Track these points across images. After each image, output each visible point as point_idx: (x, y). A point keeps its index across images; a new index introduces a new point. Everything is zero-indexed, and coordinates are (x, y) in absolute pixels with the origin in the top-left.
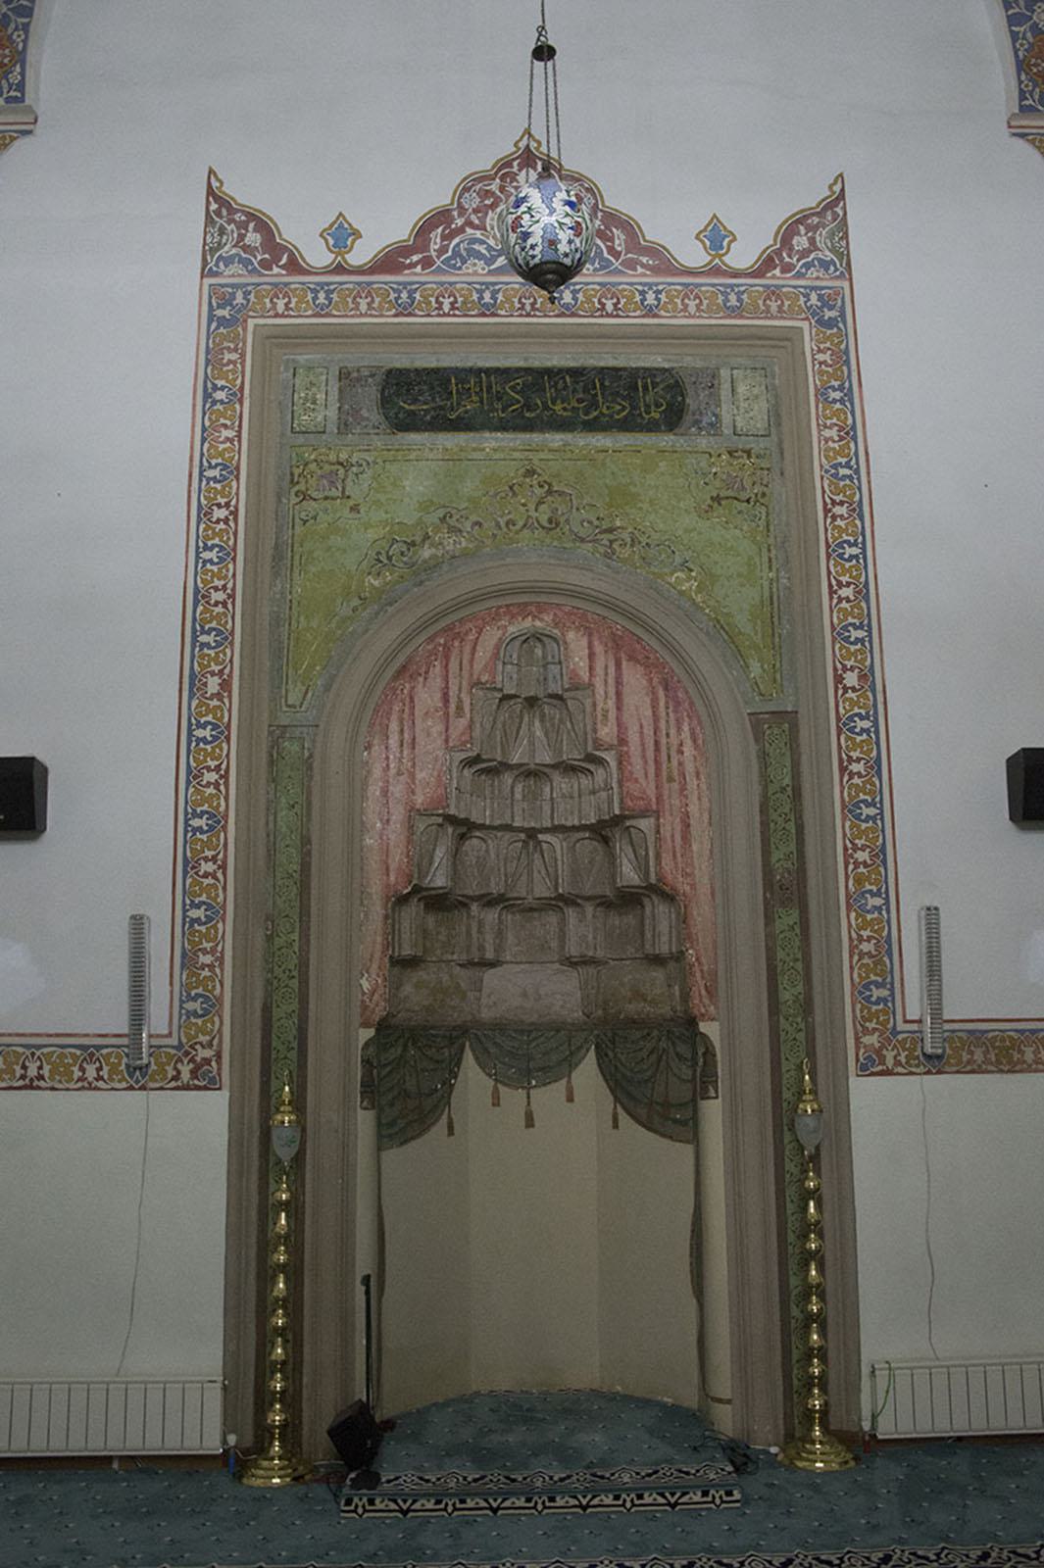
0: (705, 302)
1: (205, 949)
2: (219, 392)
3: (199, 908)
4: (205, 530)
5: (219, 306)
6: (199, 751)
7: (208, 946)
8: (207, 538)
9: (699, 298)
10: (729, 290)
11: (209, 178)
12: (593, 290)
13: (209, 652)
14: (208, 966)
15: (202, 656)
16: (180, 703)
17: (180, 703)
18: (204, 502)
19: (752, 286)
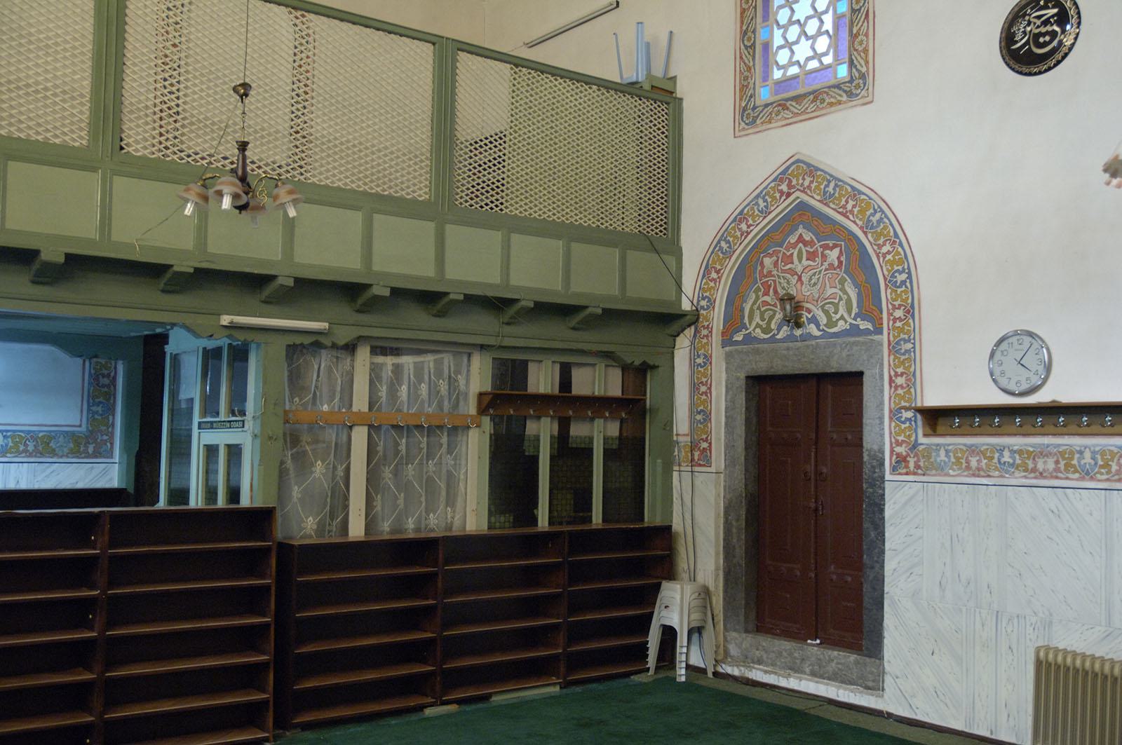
0: (896, 268)
1: (900, 321)
2: (899, 378)
3: (946, 456)
4: (908, 298)
5: (907, 467)
6: (824, 179)
7: (898, 324)
8: (910, 428)
9: (893, 274)
10: (892, 318)
11: (810, 93)
12: (891, 294)
13: (904, 336)
14: (899, 376)
15: (824, 179)
16: (901, 227)
17: (901, 227)
18: (863, 197)
19: (890, 365)
